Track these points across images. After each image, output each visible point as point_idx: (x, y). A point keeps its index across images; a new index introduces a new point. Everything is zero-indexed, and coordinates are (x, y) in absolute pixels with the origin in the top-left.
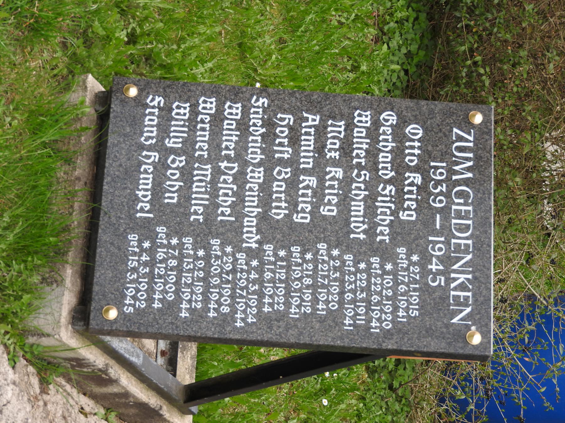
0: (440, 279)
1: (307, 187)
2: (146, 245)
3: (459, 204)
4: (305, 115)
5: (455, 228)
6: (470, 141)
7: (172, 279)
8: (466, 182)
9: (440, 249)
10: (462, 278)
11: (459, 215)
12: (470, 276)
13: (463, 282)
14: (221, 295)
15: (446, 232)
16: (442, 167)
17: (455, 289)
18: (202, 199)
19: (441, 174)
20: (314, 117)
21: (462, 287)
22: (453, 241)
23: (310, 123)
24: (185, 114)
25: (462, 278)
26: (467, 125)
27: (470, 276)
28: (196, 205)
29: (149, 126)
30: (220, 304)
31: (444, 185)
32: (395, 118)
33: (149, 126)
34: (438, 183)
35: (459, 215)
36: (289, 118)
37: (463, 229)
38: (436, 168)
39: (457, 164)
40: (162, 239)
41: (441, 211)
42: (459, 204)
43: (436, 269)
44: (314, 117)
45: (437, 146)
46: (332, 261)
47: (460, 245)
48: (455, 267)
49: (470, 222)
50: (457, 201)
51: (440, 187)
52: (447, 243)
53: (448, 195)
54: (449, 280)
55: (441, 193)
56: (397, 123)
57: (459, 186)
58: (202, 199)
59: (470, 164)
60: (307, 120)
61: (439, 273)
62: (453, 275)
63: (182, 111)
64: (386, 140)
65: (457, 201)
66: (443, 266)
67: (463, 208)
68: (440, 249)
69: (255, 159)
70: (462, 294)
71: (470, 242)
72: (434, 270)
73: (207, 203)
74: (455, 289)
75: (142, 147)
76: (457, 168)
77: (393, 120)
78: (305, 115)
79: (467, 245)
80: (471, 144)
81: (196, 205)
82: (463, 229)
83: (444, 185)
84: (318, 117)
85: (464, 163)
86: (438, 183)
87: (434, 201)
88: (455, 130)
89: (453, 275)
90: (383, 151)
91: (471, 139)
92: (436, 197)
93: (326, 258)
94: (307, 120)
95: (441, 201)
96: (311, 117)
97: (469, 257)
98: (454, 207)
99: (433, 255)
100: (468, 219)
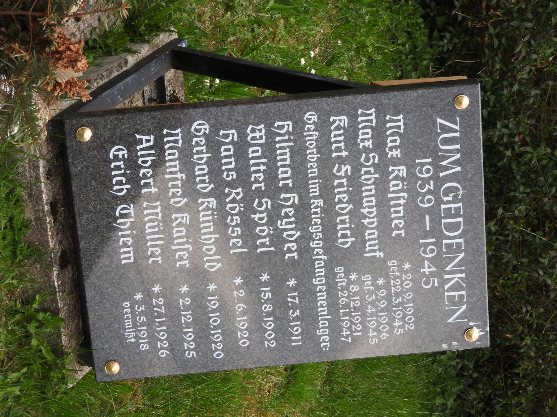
0: (434, 281)
1: (317, 207)
2: (381, 282)
3: (448, 202)
4: (138, 137)
5: (445, 228)
6: (456, 131)
7: (410, 310)
8: (453, 177)
9: (432, 251)
10: (456, 277)
11: (449, 214)
12: (463, 275)
13: (457, 282)
14: (380, 324)
15: (436, 232)
16: (428, 163)
17: (451, 289)
18: (158, 239)
19: (428, 171)
20: (148, 138)
21: (457, 287)
22: (445, 242)
23: (145, 145)
24: (261, 137)
25: (456, 277)
26: (451, 113)
27: (463, 275)
28: (152, 246)
29: (226, 157)
30: (380, 332)
31: (432, 182)
32: (207, 126)
33: (226, 157)
34: (426, 181)
35: (449, 214)
36: (233, 134)
37: (452, 227)
38: (423, 165)
39: (445, 158)
40: (395, 272)
41: (428, 210)
42: (448, 202)
43: (429, 272)
44: (148, 138)
45: (420, 142)
46: (404, 276)
47: (451, 245)
48: (448, 268)
49: (461, 219)
50: (445, 199)
51: (427, 186)
52: (438, 244)
53: (434, 192)
54: (444, 282)
55: (429, 192)
56: (210, 131)
57: (451, 182)
58: (158, 239)
59: (458, 156)
60: (141, 142)
61: (432, 274)
62: (446, 277)
63: (257, 134)
64: (201, 152)
65: (445, 199)
66: (436, 267)
67: (453, 206)
68: (432, 251)
69: (122, 190)
70: (456, 293)
71: (462, 240)
72: (427, 273)
73: (162, 242)
74: (451, 289)
75: (318, 177)
76: (444, 163)
77: (205, 129)
78: (138, 137)
79: (459, 245)
80: (457, 134)
81: (152, 246)
82: (452, 227)
83: (432, 182)
84: (152, 137)
85: (454, 156)
86: (426, 181)
87: (422, 202)
88: (439, 120)
89: (446, 277)
90: (199, 164)
91: (457, 128)
92: (424, 197)
93: (397, 274)
94: (141, 142)
95: (429, 201)
96: (144, 138)
97: (462, 255)
98: (443, 206)
99: (424, 259)
100: (459, 216)
